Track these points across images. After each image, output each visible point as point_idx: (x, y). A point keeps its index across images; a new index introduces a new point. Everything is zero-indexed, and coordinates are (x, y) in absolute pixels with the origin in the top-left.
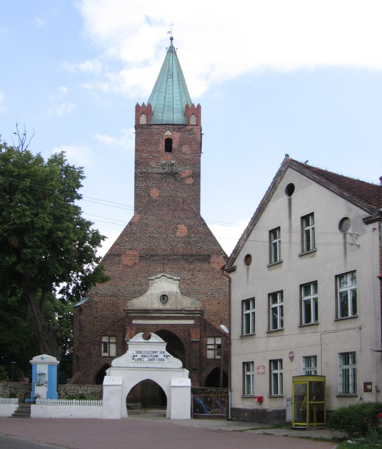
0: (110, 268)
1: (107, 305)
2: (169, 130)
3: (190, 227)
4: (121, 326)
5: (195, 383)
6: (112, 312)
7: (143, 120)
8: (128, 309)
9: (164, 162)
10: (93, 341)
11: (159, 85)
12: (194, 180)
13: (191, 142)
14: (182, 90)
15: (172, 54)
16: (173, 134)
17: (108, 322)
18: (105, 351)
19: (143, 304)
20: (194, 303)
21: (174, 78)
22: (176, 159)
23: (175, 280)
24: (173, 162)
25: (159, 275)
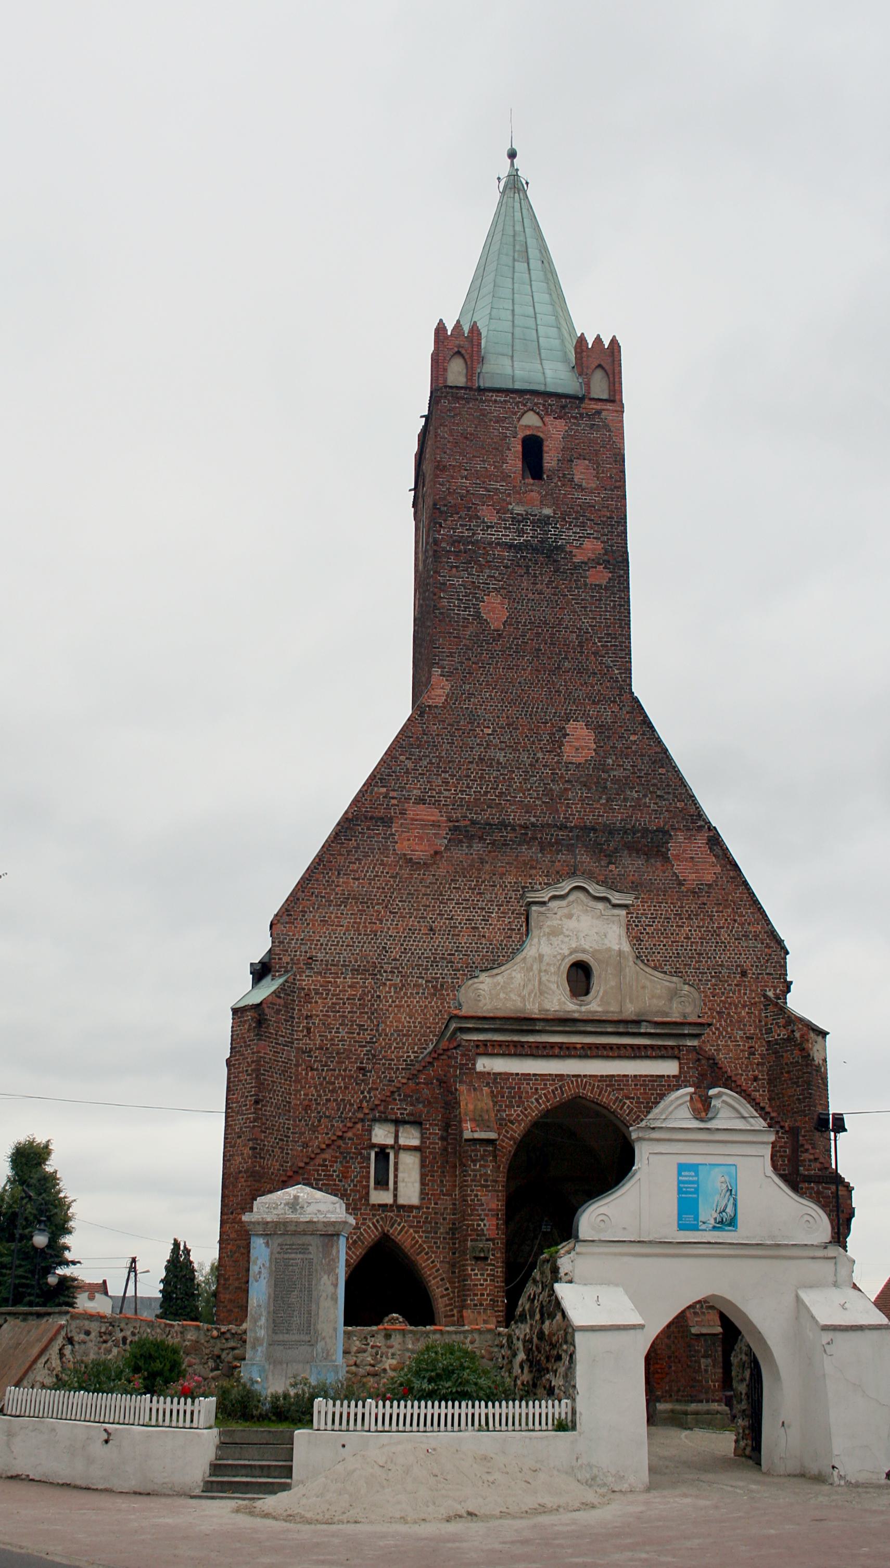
1: (344, 1004)
2: (532, 410)
3: (600, 729)
4: (437, 1080)
5: (703, 1313)
6: (359, 1034)
7: (456, 374)
8: (463, 1013)
9: (519, 509)
10: (340, 1142)
11: (489, 278)
12: (610, 575)
13: (597, 452)
14: (555, 296)
15: (517, 195)
16: (544, 422)
17: (345, 1070)
18: (382, 1183)
19: (513, 996)
20: (676, 994)
21: (531, 261)
22: (556, 504)
23: (615, 906)
24: (547, 511)
25: (566, 886)
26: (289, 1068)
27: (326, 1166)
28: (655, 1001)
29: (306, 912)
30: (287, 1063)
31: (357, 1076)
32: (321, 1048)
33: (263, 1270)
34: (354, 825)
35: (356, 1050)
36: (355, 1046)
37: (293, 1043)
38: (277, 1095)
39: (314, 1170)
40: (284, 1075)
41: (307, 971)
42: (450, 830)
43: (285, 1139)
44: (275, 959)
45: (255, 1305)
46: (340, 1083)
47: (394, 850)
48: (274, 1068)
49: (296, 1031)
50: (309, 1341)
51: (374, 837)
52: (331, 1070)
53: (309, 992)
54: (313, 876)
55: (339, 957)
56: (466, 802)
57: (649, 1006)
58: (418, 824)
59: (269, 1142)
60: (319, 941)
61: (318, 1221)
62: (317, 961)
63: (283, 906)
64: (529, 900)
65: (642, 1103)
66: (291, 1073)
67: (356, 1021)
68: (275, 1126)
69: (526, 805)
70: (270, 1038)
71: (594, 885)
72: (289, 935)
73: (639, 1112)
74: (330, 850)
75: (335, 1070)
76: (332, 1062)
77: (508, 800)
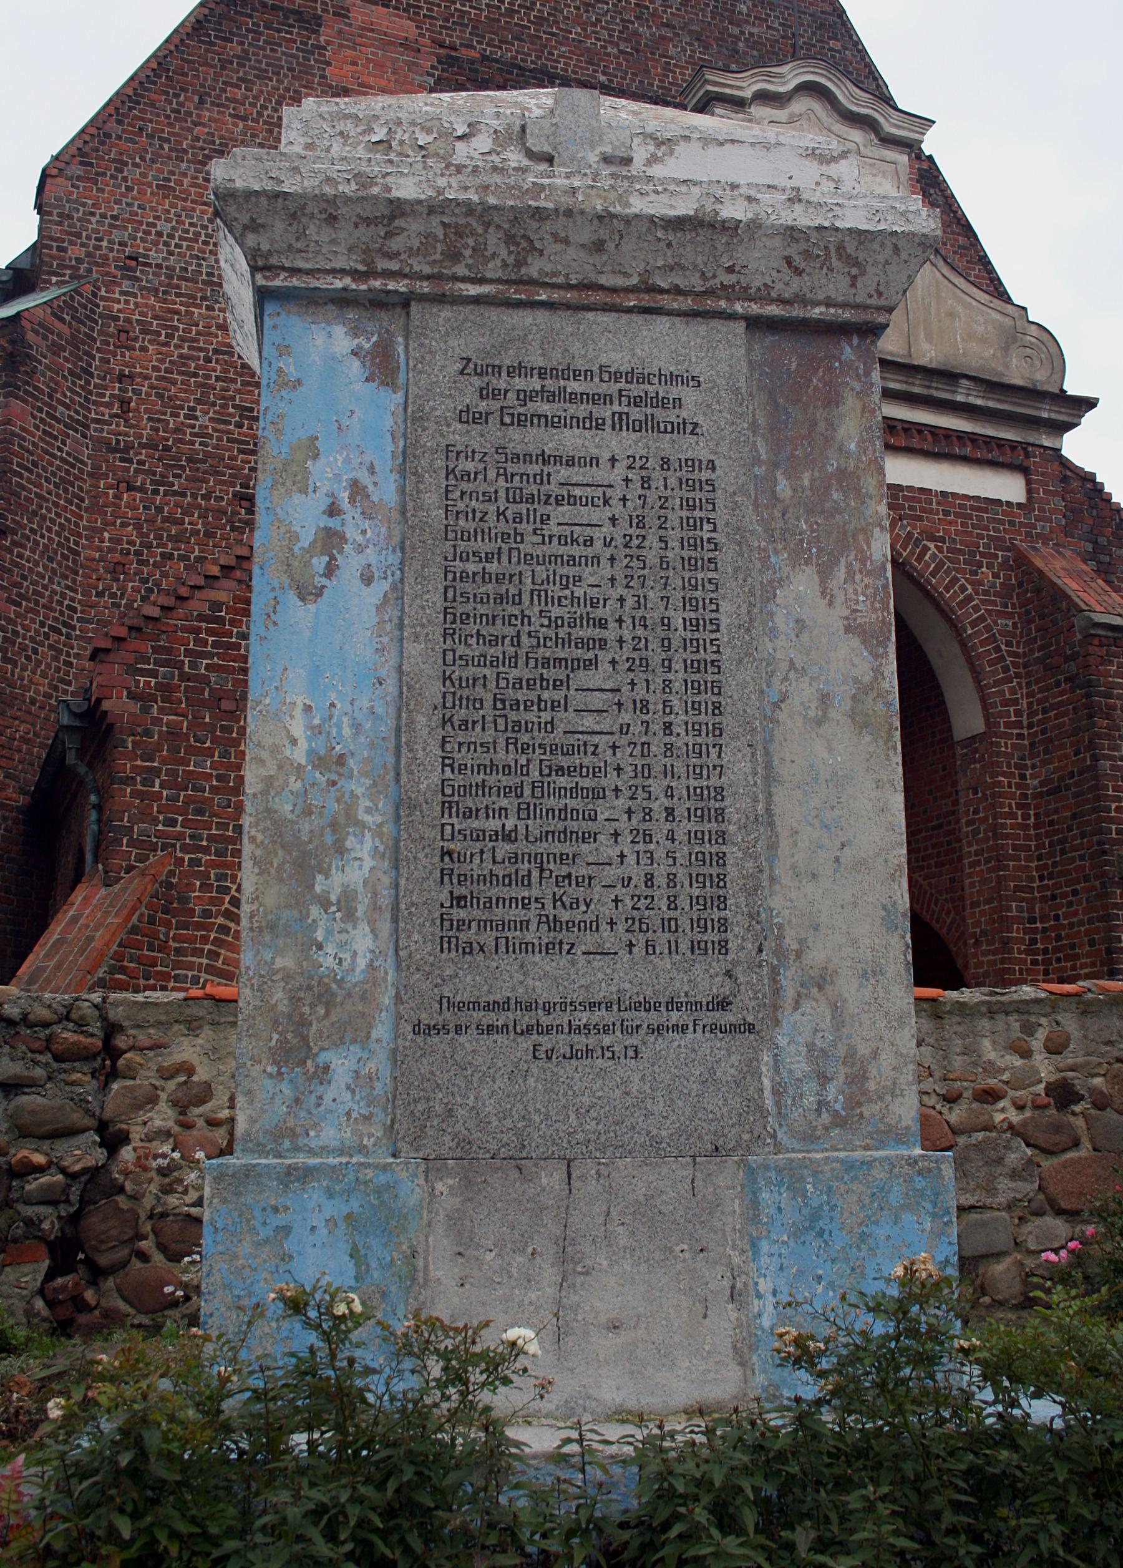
0: (239, 94)
1: (208, 360)
6: (240, 425)
25: (790, 76)
26: (77, 478)
27: (221, 621)
28: (974, 346)
29: (126, 164)
30: (73, 466)
31: (235, 513)
32: (152, 446)
33: (353, 525)
34: (236, 12)
35: (234, 458)
36: (231, 450)
37: (88, 427)
38: (49, 530)
39: (184, 629)
40: (66, 491)
41: (126, 283)
42: (439, 62)
43: (64, 630)
44: (50, 248)
45: (299, 755)
46: (194, 523)
47: (323, 77)
48: (44, 468)
49: (95, 403)
50: (723, 1004)
51: (280, 45)
52: (175, 493)
53: (128, 326)
54: (143, 97)
55: (200, 265)
56: (470, 20)
57: (965, 355)
58: (375, 39)
59: (27, 628)
60: (155, 225)
61: (755, 225)
62: (149, 265)
63: (72, 141)
64: (710, 88)
65: (961, 552)
66: (81, 489)
67: (233, 398)
68: (42, 596)
69: (588, 49)
70: (37, 399)
71: (849, 85)
72: (84, 205)
73: (957, 570)
74: (183, 52)
75: (184, 495)
76: (175, 476)
77: (553, 34)
